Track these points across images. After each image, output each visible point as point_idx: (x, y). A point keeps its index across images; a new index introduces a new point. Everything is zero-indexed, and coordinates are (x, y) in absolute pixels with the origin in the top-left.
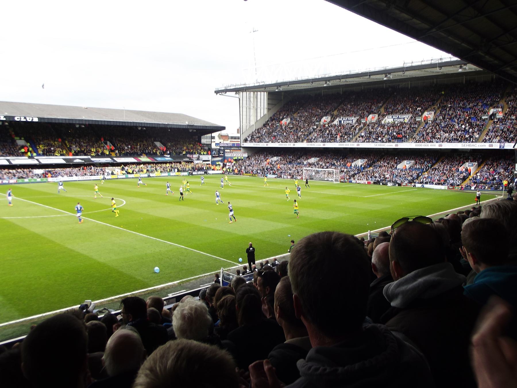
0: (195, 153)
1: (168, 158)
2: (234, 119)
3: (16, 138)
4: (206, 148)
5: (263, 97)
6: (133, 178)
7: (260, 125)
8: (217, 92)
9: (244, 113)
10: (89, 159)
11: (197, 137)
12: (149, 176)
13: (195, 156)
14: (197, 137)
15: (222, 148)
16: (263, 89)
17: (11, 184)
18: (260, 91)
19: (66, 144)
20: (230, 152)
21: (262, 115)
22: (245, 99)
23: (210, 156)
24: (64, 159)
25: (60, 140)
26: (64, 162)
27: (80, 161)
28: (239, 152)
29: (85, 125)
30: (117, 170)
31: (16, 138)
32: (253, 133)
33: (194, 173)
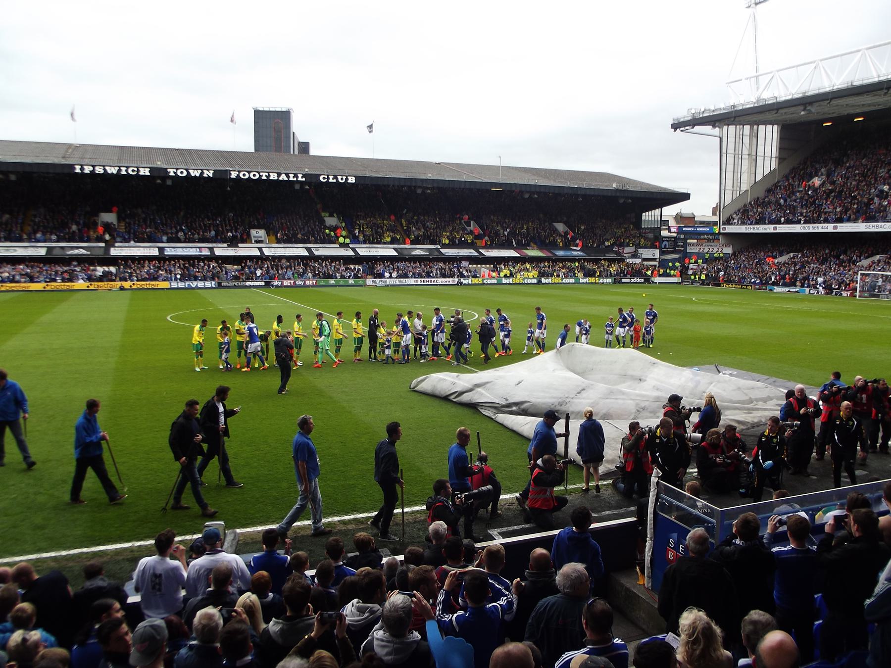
0: (628, 245)
1: (576, 252)
2: (703, 182)
3: (323, 214)
4: (651, 236)
5: (769, 137)
6: (510, 284)
7: (761, 194)
8: (676, 126)
9: (730, 168)
10: (438, 250)
11: (633, 215)
12: (539, 282)
13: (627, 250)
14: (633, 215)
15: (682, 236)
16: (771, 116)
17: (309, 286)
18: (765, 123)
19: (402, 225)
20: (697, 245)
21: (767, 171)
22: (731, 139)
23: (658, 251)
24: (395, 249)
25: (393, 218)
26: (395, 253)
27: (422, 253)
28: (716, 243)
29: (538, 193)
30: (485, 270)
31: (323, 214)
32: (745, 206)
33: (623, 280)
